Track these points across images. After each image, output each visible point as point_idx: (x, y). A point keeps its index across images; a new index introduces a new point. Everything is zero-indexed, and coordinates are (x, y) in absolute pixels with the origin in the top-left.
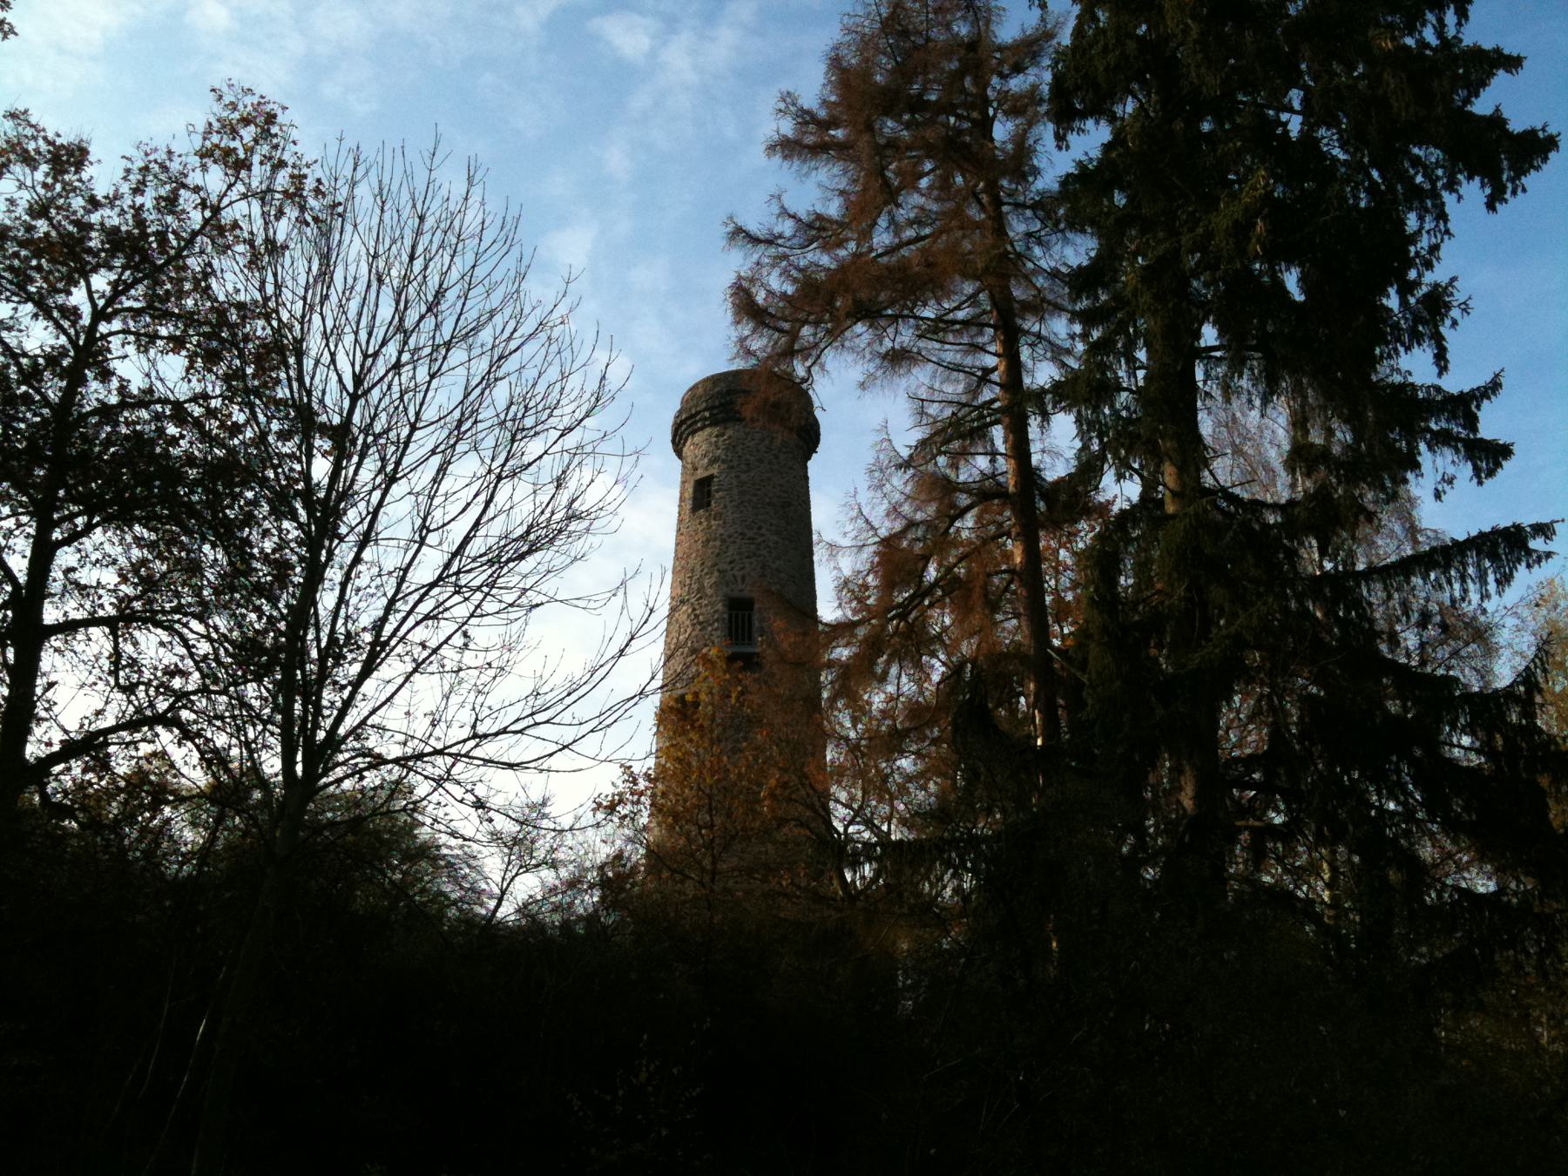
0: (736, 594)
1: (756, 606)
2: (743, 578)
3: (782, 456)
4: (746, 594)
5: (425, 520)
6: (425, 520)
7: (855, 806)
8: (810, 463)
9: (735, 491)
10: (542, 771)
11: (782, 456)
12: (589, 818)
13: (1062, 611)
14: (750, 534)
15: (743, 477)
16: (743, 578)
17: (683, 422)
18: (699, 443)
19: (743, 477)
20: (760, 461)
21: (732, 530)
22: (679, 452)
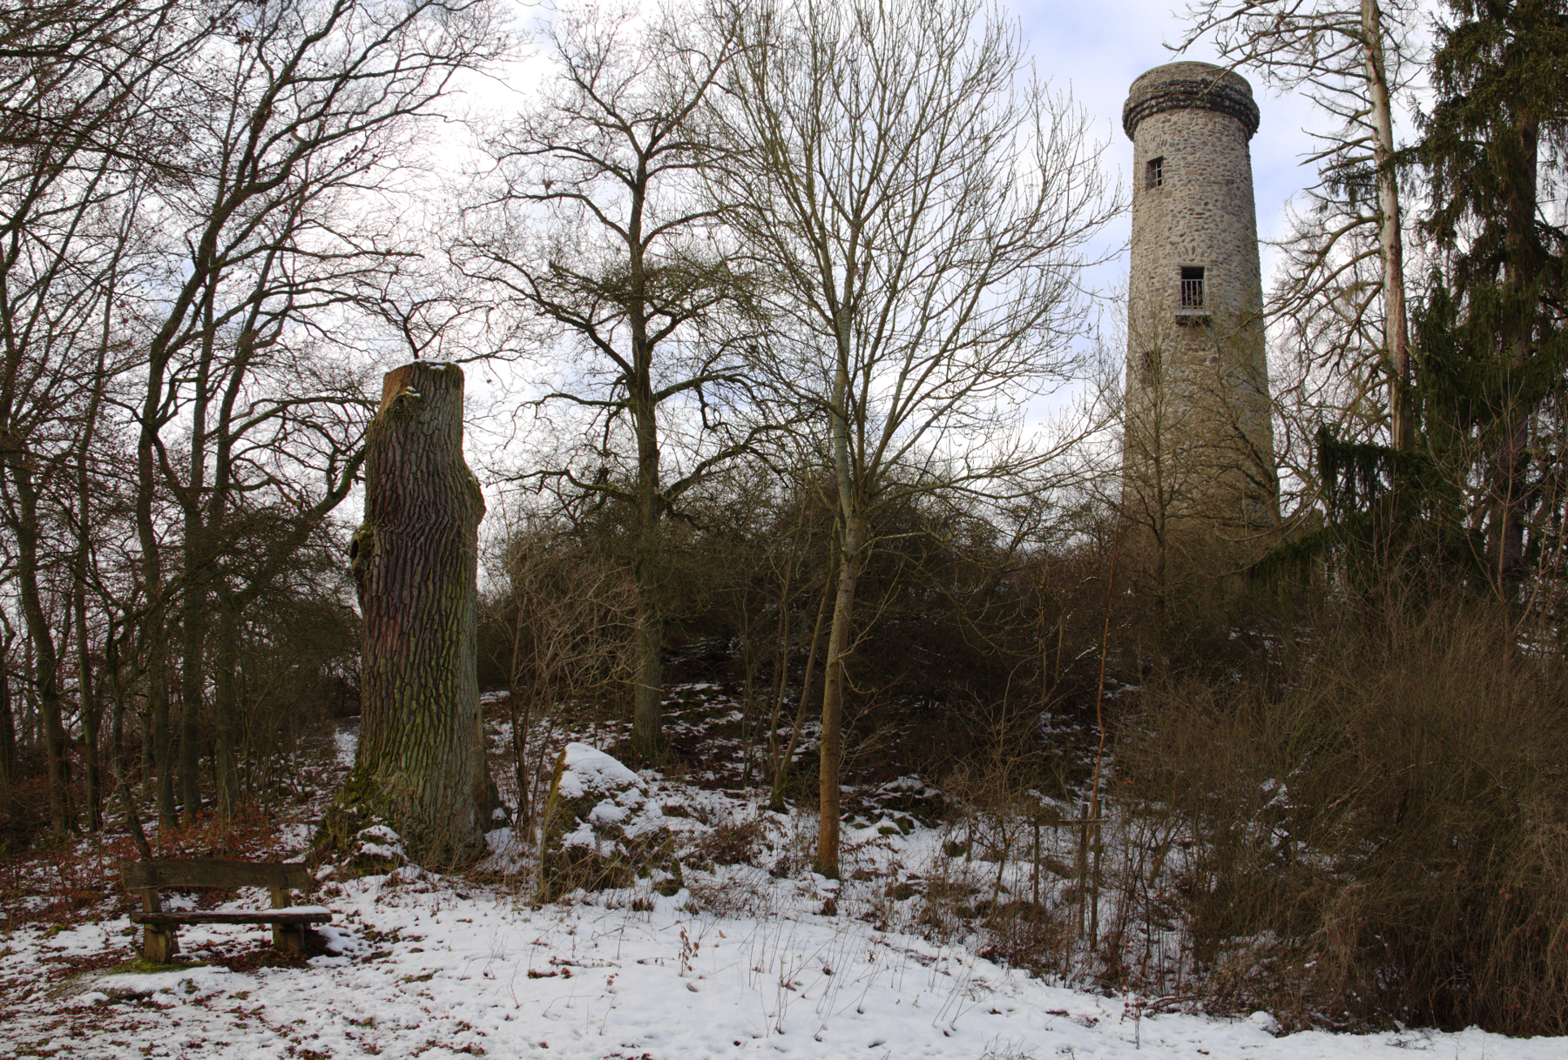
0: (1188, 263)
1: (1206, 273)
2: (1194, 249)
3: (1224, 139)
4: (1196, 263)
5: (924, 309)
6: (924, 309)
7: (591, 299)
8: (1251, 143)
9: (1183, 172)
10: (368, 167)
11: (1224, 139)
12: (580, 348)
13: (739, 266)
14: (1198, 209)
15: (1190, 159)
16: (1194, 249)
17: (1131, 110)
18: (1150, 126)
19: (1190, 159)
20: (1205, 143)
21: (1181, 207)
22: (1131, 137)
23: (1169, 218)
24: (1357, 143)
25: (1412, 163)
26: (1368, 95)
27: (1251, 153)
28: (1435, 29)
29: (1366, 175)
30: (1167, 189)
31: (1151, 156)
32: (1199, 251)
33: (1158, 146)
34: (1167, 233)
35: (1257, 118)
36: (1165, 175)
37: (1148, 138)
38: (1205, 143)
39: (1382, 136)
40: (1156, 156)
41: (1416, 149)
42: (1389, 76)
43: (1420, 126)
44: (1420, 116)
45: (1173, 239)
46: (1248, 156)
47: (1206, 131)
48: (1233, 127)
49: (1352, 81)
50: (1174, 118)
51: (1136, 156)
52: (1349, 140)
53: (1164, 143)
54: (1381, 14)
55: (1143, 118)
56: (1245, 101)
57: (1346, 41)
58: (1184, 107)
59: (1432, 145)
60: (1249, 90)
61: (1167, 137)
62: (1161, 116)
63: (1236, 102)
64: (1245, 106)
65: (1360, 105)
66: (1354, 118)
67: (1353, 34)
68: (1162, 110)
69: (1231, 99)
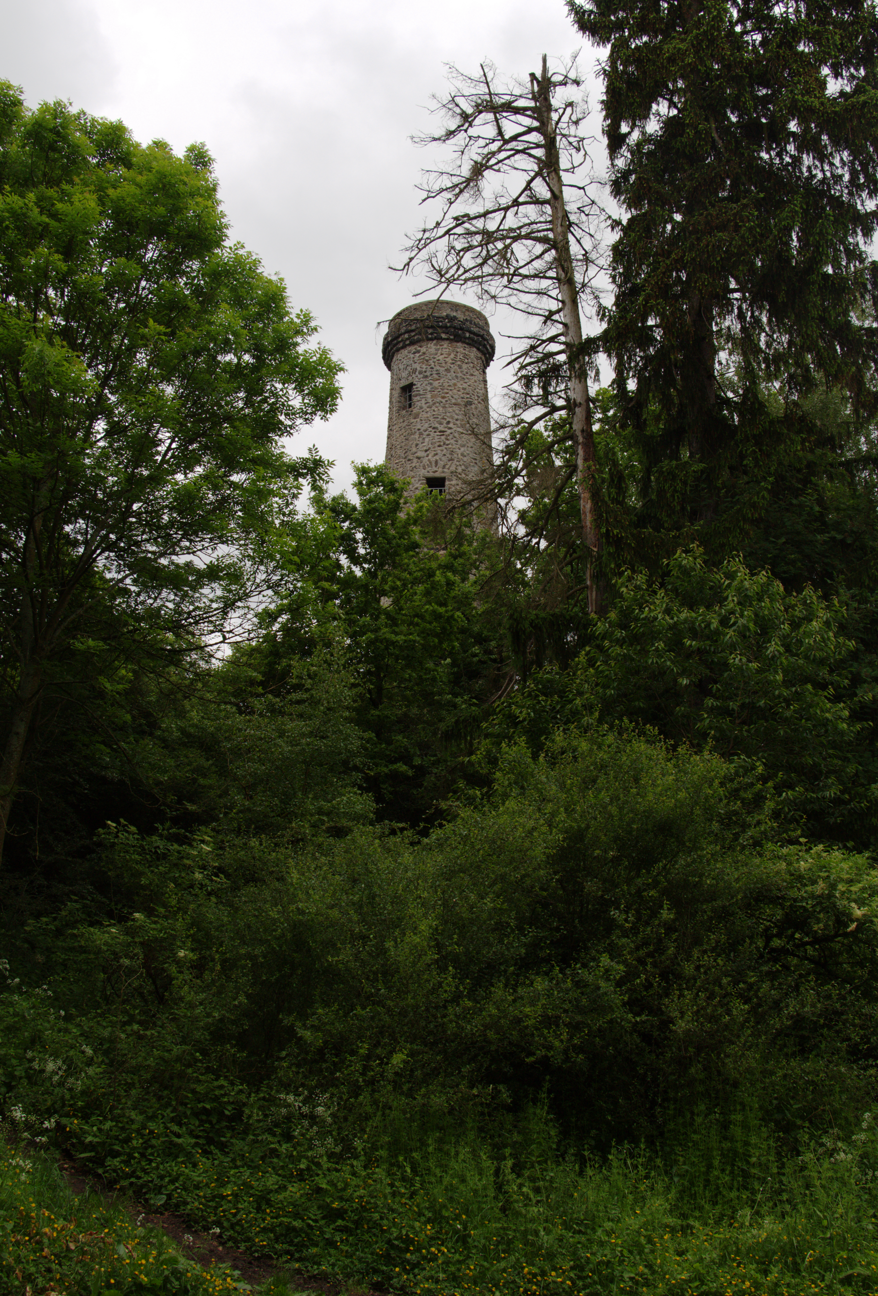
0: (431, 475)
1: (447, 483)
2: (436, 462)
8: (488, 370)
9: (429, 396)
16: (436, 462)
20: (448, 370)
23: (417, 436)
24: (552, 339)
25: (596, 352)
26: (560, 297)
27: (488, 379)
28: (609, 222)
29: (556, 368)
30: (415, 411)
31: (404, 383)
32: (441, 463)
33: (409, 375)
34: (414, 449)
35: (493, 348)
36: (415, 399)
37: (401, 367)
38: (448, 370)
39: (571, 332)
40: (407, 383)
41: (620, 358)
42: (578, 277)
43: (602, 320)
44: (602, 312)
45: (419, 454)
46: (485, 381)
47: (449, 360)
48: (472, 355)
49: (545, 284)
50: (423, 350)
51: (392, 383)
52: (544, 338)
53: (415, 371)
54: (571, 224)
55: (398, 350)
56: (482, 332)
57: (539, 248)
58: (432, 340)
59: (613, 334)
60: (487, 324)
61: (417, 366)
62: (412, 348)
63: (474, 334)
64: (482, 336)
65: (554, 306)
66: (549, 317)
67: (543, 240)
68: (412, 343)
69: (471, 332)
